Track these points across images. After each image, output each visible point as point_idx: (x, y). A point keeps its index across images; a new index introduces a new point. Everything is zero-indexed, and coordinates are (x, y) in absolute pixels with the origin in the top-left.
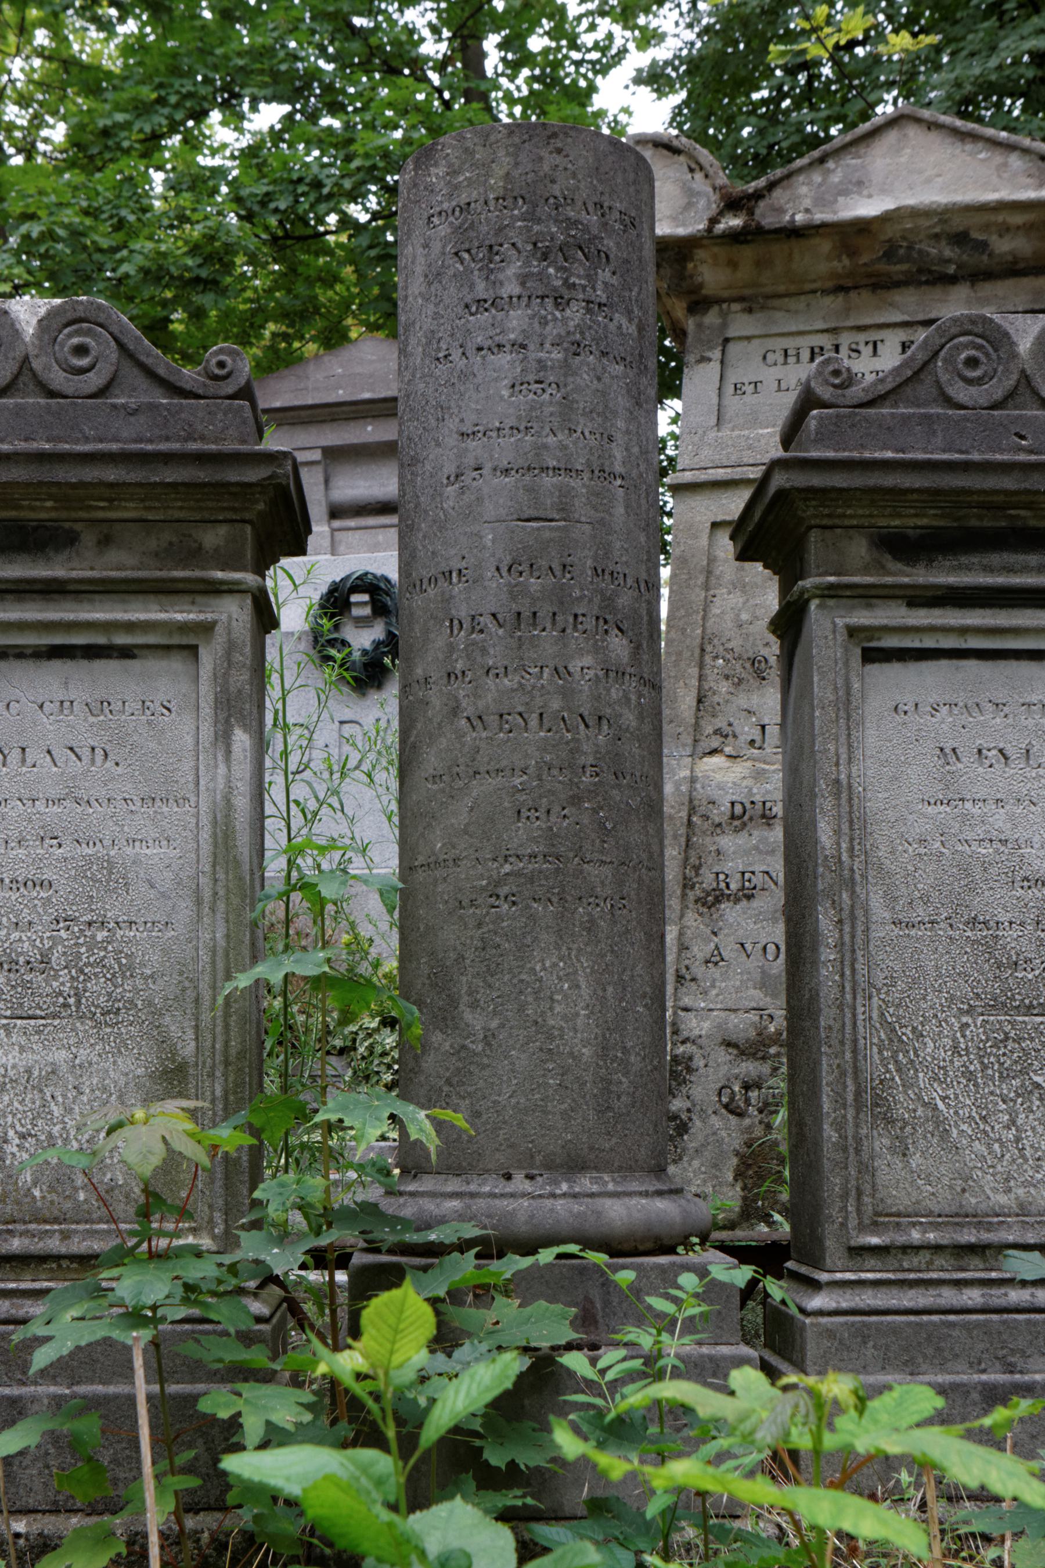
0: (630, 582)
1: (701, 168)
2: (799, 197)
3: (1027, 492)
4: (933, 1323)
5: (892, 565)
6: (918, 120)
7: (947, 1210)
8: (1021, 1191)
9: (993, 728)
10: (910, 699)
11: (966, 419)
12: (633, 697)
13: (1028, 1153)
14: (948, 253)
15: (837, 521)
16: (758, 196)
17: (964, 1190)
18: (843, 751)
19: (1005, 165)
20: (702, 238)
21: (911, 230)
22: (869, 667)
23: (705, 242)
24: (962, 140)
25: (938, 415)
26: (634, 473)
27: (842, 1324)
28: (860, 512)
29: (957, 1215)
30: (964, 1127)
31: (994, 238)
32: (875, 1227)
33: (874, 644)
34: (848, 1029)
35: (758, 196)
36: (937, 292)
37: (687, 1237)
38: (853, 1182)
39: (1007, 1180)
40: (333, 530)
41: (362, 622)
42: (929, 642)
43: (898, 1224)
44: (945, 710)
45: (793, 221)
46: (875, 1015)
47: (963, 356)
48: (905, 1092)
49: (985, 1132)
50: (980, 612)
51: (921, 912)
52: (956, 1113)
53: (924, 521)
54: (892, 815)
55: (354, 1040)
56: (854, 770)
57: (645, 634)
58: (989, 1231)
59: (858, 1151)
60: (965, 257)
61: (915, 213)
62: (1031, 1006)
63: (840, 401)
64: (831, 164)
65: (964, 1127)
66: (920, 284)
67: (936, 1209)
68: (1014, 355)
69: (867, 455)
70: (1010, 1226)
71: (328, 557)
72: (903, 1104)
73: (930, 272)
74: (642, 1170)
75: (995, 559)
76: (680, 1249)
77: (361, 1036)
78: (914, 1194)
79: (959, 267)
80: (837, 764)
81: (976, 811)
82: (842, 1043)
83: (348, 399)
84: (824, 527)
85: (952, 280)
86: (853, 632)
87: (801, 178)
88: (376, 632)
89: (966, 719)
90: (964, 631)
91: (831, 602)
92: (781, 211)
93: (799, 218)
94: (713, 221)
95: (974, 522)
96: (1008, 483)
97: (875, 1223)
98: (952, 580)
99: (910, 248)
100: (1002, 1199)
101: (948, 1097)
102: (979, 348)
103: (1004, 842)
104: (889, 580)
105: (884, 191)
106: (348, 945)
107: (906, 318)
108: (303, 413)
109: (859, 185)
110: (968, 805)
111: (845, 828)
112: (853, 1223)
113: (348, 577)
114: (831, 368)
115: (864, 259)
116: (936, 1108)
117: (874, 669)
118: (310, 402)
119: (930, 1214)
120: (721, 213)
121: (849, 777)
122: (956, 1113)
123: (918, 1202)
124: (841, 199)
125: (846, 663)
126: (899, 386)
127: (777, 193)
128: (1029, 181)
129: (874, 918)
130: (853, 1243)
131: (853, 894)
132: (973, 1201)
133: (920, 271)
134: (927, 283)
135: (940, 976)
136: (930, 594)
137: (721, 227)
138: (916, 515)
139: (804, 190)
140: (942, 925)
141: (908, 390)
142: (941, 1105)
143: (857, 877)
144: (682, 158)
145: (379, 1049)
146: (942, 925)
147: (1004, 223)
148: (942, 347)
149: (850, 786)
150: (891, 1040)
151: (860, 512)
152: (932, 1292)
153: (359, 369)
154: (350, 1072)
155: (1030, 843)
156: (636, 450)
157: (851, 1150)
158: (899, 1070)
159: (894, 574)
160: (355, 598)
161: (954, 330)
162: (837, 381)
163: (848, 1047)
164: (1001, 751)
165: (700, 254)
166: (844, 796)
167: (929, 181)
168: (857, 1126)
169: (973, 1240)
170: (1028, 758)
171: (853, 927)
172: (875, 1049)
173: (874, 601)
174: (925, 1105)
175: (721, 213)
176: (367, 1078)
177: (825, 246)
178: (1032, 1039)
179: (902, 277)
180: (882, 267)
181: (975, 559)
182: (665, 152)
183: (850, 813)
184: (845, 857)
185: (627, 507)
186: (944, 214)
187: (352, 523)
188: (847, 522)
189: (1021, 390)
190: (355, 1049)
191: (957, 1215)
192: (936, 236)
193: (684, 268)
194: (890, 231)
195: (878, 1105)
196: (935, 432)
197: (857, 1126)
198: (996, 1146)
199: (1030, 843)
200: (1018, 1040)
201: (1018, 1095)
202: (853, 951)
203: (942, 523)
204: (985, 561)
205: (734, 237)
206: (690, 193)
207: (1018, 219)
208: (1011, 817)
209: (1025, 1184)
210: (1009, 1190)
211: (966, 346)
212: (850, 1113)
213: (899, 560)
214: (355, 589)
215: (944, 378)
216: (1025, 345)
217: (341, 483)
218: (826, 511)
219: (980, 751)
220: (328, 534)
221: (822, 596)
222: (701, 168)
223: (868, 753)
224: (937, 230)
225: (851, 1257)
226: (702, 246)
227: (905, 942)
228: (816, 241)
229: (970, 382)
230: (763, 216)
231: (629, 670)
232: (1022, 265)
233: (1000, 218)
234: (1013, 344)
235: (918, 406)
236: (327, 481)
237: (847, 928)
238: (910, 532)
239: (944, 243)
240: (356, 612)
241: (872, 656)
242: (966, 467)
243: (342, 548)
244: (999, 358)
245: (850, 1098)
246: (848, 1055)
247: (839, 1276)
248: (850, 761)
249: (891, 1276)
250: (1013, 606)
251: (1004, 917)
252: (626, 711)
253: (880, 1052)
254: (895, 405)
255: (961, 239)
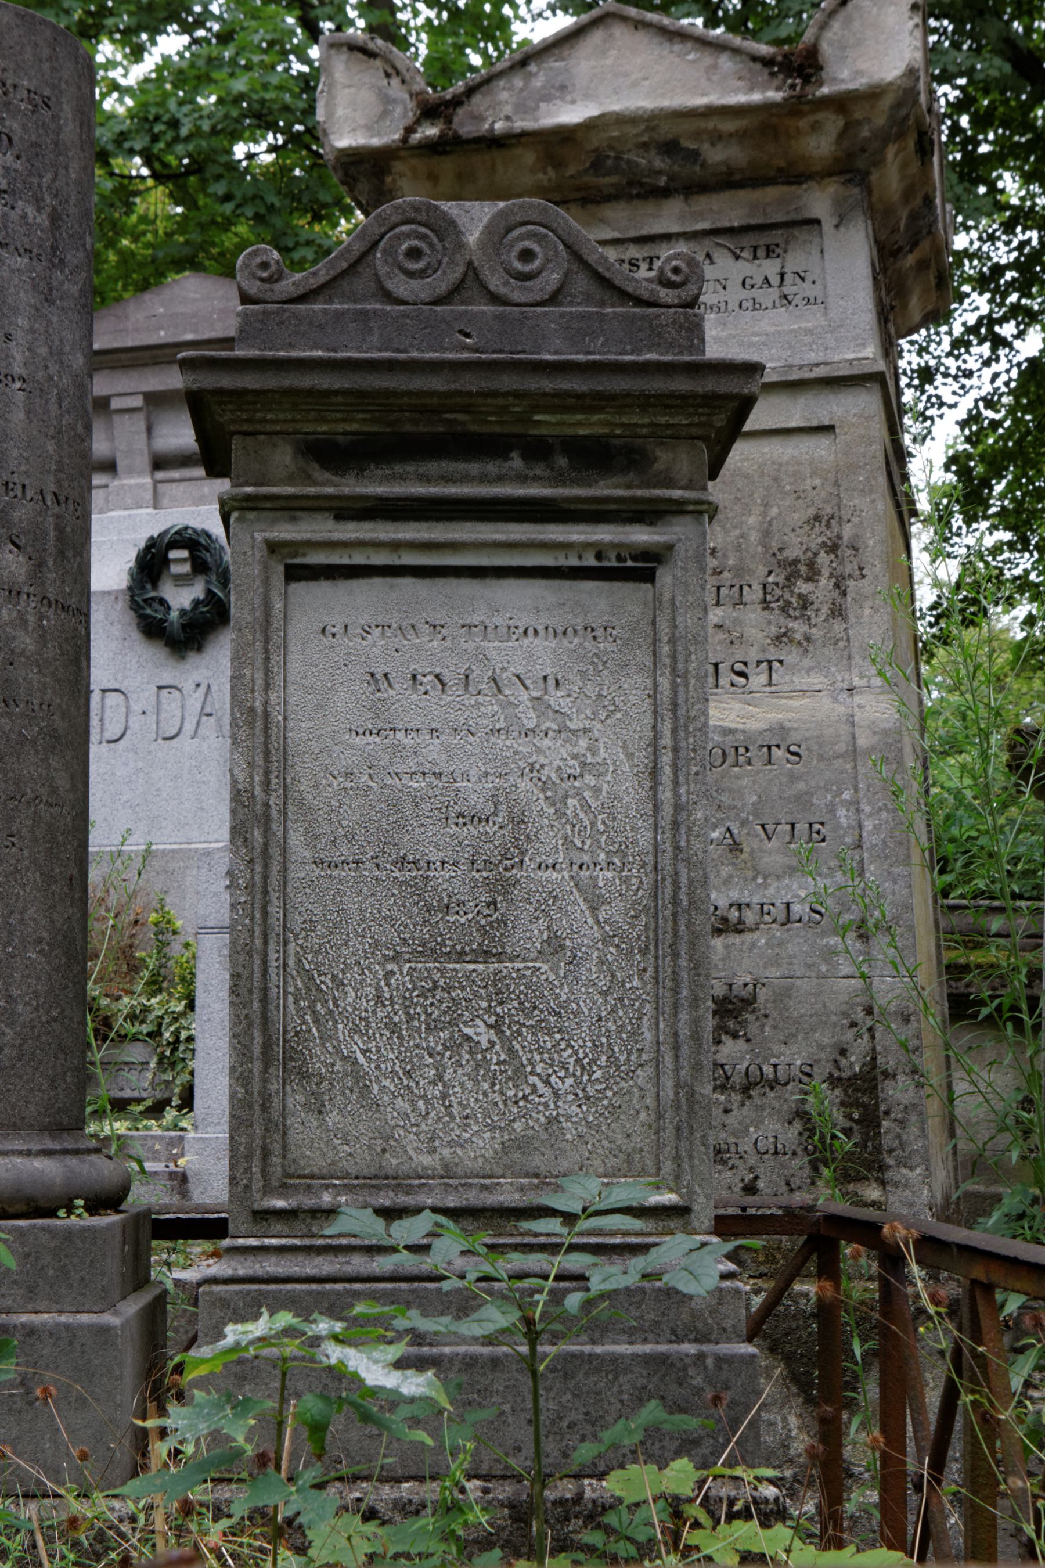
0: (29, 494)
1: (398, 73)
2: (500, 103)
3: (458, 393)
4: (338, 1293)
5: (319, 474)
6: (625, 19)
7: (365, 1172)
8: (446, 1152)
9: (428, 652)
10: (339, 620)
11: (405, 315)
12: (31, 619)
13: (455, 1111)
14: (658, 163)
15: (259, 427)
16: (457, 102)
17: (384, 1151)
18: (259, 677)
19: (715, 66)
20: (398, 149)
21: (617, 139)
22: (294, 586)
23: (403, 153)
24: (671, 40)
25: (375, 311)
26: (41, 375)
27: (237, 1293)
28: (281, 416)
29: (376, 1177)
30: (386, 1083)
31: (706, 146)
32: (284, 1189)
33: (298, 561)
34: (257, 976)
35: (457, 102)
36: (649, 207)
37: (71, 1200)
38: (259, 1142)
39: (432, 1140)
40: (156, 483)
41: (181, 580)
42: (359, 558)
43: (309, 1186)
44: (377, 632)
45: (492, 129)
46: (291, 961)
47: (404, 247)
48: (323, 1045)
49: (408, 1087)
50: (414, 525)
51: (345, 851)
52: (378, 1067)
53: (354, 427)
54: (315, 746)
55: (160, 1025)
56: (273, 697)
57: (52, 550)
58: (408, 1194)
59: (264, 1108)
60: (676, 168)
61: (620, 119)
62: (463, 953)
63: (268, 296)
64: (533, 68)
65: (386, 1083)
66: (631, 198)
67: (354, 1171)
68: (461, 246)
69: (294, 354)
70: (431, 1189)
71: (151, 510)
72: (320, 1058)
73: (641, 185)
74: (31, 1127)
75: (433, 467)
76: (62, 1213)
77: (167, 1020)
78: (330, 1154)
79: (671, 178)
80: (253, 691)
81: (408, 741)
82: (250, 991)
83: (170, 340)
84: (246, 434)
85: (664, 193)
86: (273, 547)
87: (502, 83)
88: (197, 591)
89: (400, 641)
90: (396, 546)
91: (251, 515)
92: (481, 119)
93: (499, 126)
94: (409, 130)
95: (409, 428)
96: (437, 383)
97: (284, 1186)
98: (380, 490)
99: (618, 158)
100: (426, 1160)
101: (369, 1050)
102: (423, 237)
103: (439, 775)
104: (312, 490)
105: (588, 96)
106: (156, 924)
107: (617, 235)
108: (123, 356)
109: (561, 90)
110: (400, 735)
111: (259, 759)
112: (257, 1184)
113: (166, 532)
114: (258, 260)
115: (571, 170)
116: (356, 1062)
117: (298, 588)
118: (130, 343)
119: (347, 1175)
120: (418, 122)
121: (266, 704)
122: (378, 1067)
123: (333, 1163)
124: (543, 105)
125: (266, 582)
126: (334, 279)
127: (477, 99)
128: (740, 83)
129: (294, 858)
130: (256, 1207)
131: (267, 831)
132: (394, 1162)
133: (630, 184)
134: (639, 196)
135: (364, 920)
136: (359, 505)
137: (417, 136)
138: (344, 420)
139: (504, 95)
140: (368, 865)
141: (345, 284)
142: (361, 1059)
143: (274, 813)
144: (378, 63)
145: (183, 1035)
146: (368, 865)
147: (715, 129)
148: (382, 236)
149: (266, 715)
150: (308, 989)
151: (281, 416)
152: (341, 1259)
153: (181, 309)
154: (155, 1059)
155: (466, 776)
156: (43, 351)
157: (257, 1107)
158: (316, 1021)
159: (315, 484)
160: (173, 554)
161: (395, 219)
162: (265, 275)
163: (256, 995)
164: (437, 676)
165: (398, 166)
166: (259, 724)
167: (635, 85)
168: (265, 1081)
169: (388, 1203)
170: (467, 685)
171: (266, 866)
172: (291, 999)
173: (299, 514)
174: (344, 1058)
175: (418, 122)
176: (173, 1065)
177: (529, 157)
178: (463, 988)
179: (613, 191)
180: (590, 179)
181: (410, 468)
182: (360, 56)
183: (266, 744)
184: (258, 791)
185: (28, 412)
186: (652, 120)
187: (176, 474)
188: (269, 428)
189: (468, 283)
190: (161, 1035)
191: (376, 1177)
192: (645, 146)
193: (383, 182)
194: (596, 141)
195: (292, 1059)
196: (371, 329)
197: (265, 1081)
198: (421, 1103)
199: (466, 776)
200: (448, 989)
201: (446, 1048)
202: (266, 893)
203: (374, 429)
204: (421, 470)
205: (431, 147)
206: (387, 100)
207: (729, 126)
208: (447, 749)
209: (451, 1144)
210: (434, 1150)
211: (408, 236)
212: (257, 1067)
213: (327, 469)
214: (174, 544)
215: (383, 270)
216: (473, 237)
217: (165, 431)
218: (244, 416)
219: (414, 677)
220: (150, 486)
221: (241, 509)
222: (398, 73)
223: (291, 678)
224: (645, 138)
225: (255, 1221)
226: (399, 158)
227: (327, 883)
228: (518, 151)
229: (411, 274)
230: (462, 124)
231: (26, 589)
232: (737, 177)
233: (711, 125)
234: (459, 233)
235: (355, 302)
236: (149, 430)
237: (258, 868)
238: (340, 438)
239: (653, 152)
240: (175, 569)
241: (296, 574)
242: (390, 366)
243: (165, 501)
244: (444, 248)
245: (257, 1050)
246: (256, 1005)
247: (241, 1241)
248: (267, 686)
249: (297, 1242)
250: (451, 519)
251: (435, 857)
252: (20, 633)
253: (296, 1002)
254: (330, 300)
255: (670, 148)
